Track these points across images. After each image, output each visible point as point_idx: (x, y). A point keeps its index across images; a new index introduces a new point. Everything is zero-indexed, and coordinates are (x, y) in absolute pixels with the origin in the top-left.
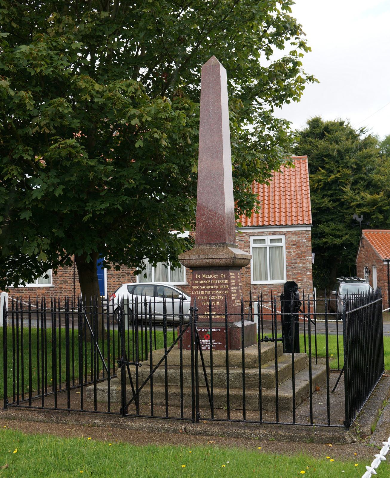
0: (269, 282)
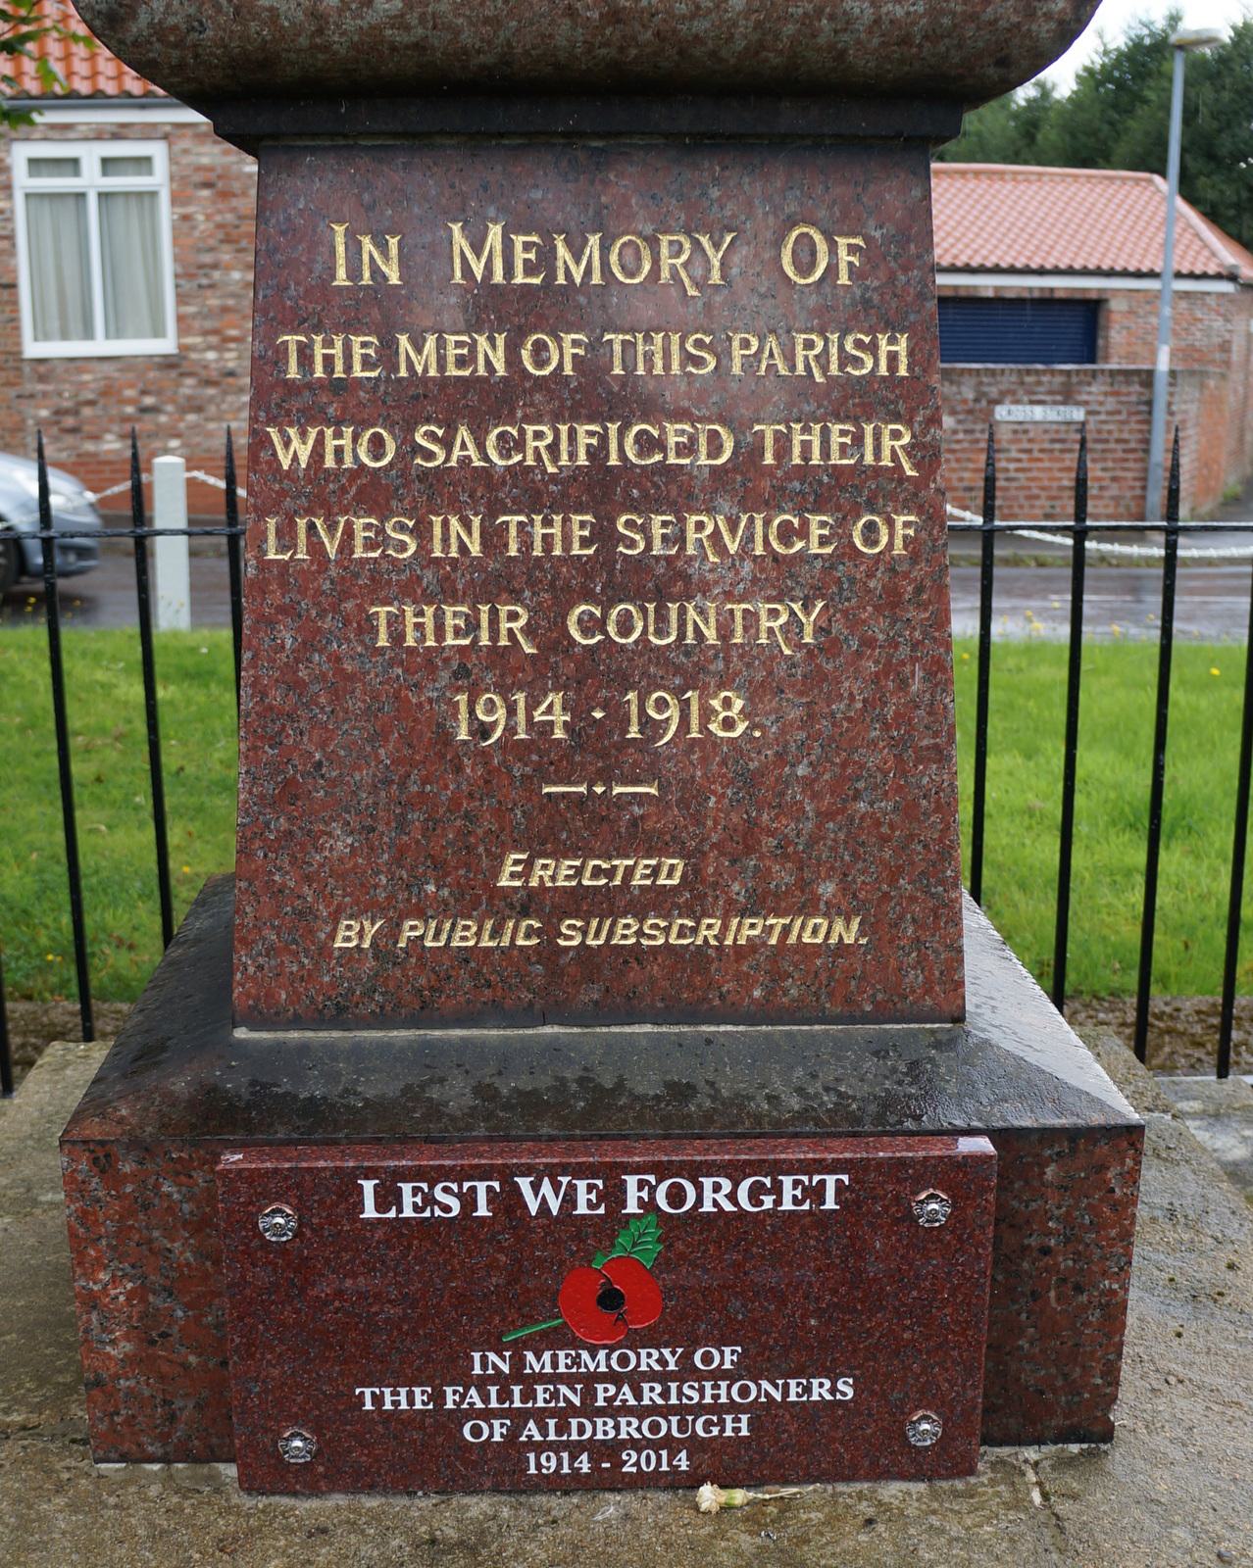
0: (101, 346)
